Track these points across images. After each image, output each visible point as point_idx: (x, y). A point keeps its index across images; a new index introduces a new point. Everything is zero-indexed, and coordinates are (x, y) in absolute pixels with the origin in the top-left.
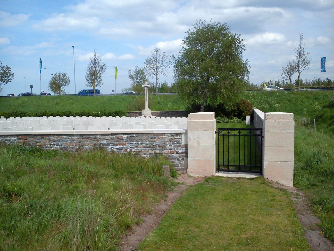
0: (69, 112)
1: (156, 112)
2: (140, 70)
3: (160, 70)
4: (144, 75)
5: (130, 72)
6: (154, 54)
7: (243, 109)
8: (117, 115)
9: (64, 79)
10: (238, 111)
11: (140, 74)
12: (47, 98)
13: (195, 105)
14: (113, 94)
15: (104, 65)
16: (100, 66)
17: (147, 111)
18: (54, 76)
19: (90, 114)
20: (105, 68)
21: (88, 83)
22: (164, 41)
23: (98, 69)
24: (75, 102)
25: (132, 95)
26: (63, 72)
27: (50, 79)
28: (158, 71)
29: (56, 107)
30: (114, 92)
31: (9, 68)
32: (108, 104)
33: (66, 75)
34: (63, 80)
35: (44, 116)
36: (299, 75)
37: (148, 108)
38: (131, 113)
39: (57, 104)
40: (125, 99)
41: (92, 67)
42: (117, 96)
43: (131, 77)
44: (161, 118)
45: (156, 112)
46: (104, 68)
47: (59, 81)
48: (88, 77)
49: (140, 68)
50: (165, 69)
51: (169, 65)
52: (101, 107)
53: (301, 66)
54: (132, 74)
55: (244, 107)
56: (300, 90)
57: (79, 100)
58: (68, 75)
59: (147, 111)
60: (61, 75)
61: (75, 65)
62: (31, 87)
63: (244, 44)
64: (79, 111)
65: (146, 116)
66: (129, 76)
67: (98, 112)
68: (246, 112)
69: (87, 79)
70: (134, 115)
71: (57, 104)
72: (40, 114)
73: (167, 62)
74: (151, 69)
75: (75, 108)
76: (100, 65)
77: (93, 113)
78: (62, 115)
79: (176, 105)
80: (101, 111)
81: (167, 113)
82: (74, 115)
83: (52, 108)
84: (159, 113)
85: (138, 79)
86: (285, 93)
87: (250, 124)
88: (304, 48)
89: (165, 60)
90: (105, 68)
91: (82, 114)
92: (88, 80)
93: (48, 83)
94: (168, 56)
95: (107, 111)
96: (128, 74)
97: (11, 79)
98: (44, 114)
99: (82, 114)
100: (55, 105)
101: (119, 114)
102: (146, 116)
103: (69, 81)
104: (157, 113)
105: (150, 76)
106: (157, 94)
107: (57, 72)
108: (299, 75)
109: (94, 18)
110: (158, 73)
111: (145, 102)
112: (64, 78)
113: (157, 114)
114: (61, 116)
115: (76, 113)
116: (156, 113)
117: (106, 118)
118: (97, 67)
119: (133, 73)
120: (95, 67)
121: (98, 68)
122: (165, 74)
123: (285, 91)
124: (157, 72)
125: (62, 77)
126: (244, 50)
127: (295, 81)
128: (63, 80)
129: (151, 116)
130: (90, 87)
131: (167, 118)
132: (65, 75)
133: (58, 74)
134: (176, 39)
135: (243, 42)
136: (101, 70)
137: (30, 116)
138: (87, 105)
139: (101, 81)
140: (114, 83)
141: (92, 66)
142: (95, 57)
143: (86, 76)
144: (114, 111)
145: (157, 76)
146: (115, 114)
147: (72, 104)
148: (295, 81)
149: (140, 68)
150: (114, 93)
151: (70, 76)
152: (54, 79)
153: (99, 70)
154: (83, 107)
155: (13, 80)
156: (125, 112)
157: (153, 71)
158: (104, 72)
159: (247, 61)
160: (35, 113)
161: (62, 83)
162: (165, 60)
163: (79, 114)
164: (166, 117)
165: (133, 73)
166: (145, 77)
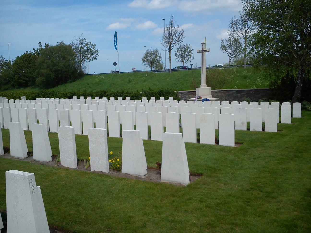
1: (223, 92)
13: (225, 70)
23: (174, 38)
31: (94, 46)
37: (206, 85)
38: (185, 93)
39: (130, 81)
42: (195, 70)
45: (222, 92)
58: (159, 51)
64: (156, 89)
70: (190, 95)
71: (130, 81)
81: (256, 92)
96: (221, 46)
97: (97, 57)
106: (245, 65)
107: (149, 49)
111: (201, 74)
116: (222, 93)
119: (226, 43)
132: (157, 51)
147: (145, 81)
155: (98, 57)
164: (240, 100)
165: (226, 43)
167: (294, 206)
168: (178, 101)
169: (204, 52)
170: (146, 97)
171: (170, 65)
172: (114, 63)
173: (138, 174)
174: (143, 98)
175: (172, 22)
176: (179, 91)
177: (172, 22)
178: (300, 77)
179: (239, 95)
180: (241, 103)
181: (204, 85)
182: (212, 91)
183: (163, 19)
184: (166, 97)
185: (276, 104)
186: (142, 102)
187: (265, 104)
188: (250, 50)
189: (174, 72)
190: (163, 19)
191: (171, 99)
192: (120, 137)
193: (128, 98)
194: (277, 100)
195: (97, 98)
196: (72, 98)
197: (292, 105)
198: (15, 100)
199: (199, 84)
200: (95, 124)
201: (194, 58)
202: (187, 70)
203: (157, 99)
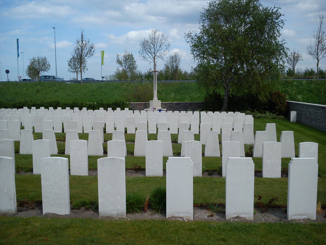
0: (56, 102)
1: (165, 104)
2: (129, 55)
3: (158, 54)
4: (134, 60)
5: (118, 57)
6: (152, 35)
7: (276, 101)
8: (118, 107)
9: (44, 64)
10: (269, 104)
11: (129, 59)
12: (26, 85)
14: (103, 81)
15: (92, 48)
16: (88, 49)
17: (156, 103)
18: (33, 61)
19: (83, 105)
20: (94, 51)
21: (70, 68)
22: (136, 30)
23: (85, 51)
24: (59, 89)
25: (125, 82)
26: (42, 55)
27: (27, 64)
28: (156, 55)
29: (36, 95)
30: (103, 78)
32: (98, 93)
33: (46, 59)
34: (43, 65)
35: (24, 107)
36: (318, 62)
38: (134, 105)
40: (117, 87)
41: (78, 49)
43: (119, 62)
44: (180, 112)
46: (92, 50)
47: (39, 66)
48: (70, 61)
49: (129, 53)
50: (164, 53)
51: (168, 48)
52: (90, 95)
53: (320, 53)
54: (120, 59)
55: (277, 99)
56: (318, 79)
57: (64, 87)
58: (48, 60)
59: (156, 103)
60: (41, 59)
61: (55, 48)
62: (7, 72)
63: (282, 20)
64: (112, 100)
65: (155, 109)
66: (117, 62)
67: (93, 102)
68: (280, 105)
69: (69, 65)
70: (138, 106)
71: (38, 91)
72: (19, 104)
73: (166, 45)
74: (148, 53)
75: (59, 96)
76: (88, 46)
77: (87, 104)
78: (47, 106)
79: (178, 95)
80: (97, 102)
81: (190, 104)
82: (63, 105)
83: (31, 96)
84: (168, 105)
85: (127, 64)
86: (303, 83)
87: (296, 121)
88: (324, 33)
89: (164, 43)
90: (94, 51)
91: (73, 104)
92: (71, 65)
93: (26, 68)
94: (167, 39)
95: (105, 102)
96: (116, 60)
98: (24, 105)
99: (73, 104)
100: (36, 93)
101: (121, 106)
102: (155, 109)
103: (50, 66)
104: (166, 104)
105: (146, 61)
108: (318, 62)
109: (66, 6)
110: (156, 57)
112: (43, 63)
113: (166, 105)
114: (47, 107)
115: (65, 103)
116: (165, 105)
117: (69, 110)
118: (84, 49)
119: (121, 58)
120: (82, 50)
121: (85, 50)
122: (163, 59)
123: (304, 81)
124: (155, 57)
125: (42, 61)
126: (282, 28)
127: (287, 70)
128: (43, 65)
129: (160, 108)
130: (73, 73)
131: (134, 111)
132: (45, 59)
133: (37, 59)
134: (148, 29)
135: (282, 18)
136: (89, 53)
137: (6, 108)
138: (73, 93)
139: (86, 67)
140: (101, 68)
141: (79, 48)
142: (82, 38)
143: (69, 61)
144: (114, 102)
145: (154, 61)
146: (116, 105)
147: (56, 91)
148: (287, 70)
149: (129, 53)
150: (104, 79)
151: (51, 61)
152: (33, 63)
153: (86, 53)
154: (69, 95)
156: (127, 103)
157: (150, 54)
158: (93, 55)
159: (284, 42)
160: (13, 103)
161: (41, 68)
162: (164, 43)
163: (70, 106)
164: (186, 110)
165: (121, 58)
166: (135, 63)
167: (79, 226)
168: (12, 109)
169: (156, 72)
170: (103, 108)
171: (81, 77)
172: (9, 73)
173: (252, 144)
174: (100, 108)
175: (82, 36)
176: (130, 103)
177: (82, 36)
178: (226, 94)
179: (178, 107)
180: (214, 112)
181: (156, 98)
182: (161, 103)
183: (54, 28)
184: (122, 108)
185: (197, 113)
186: (48, 110)
187: (190, 113)
188: (120, 60)
189: (86, 84)
190: (54, 28)
191: (127, 109)
192: (156, 133)
193: (84, 109)
194: (197, 110)
195: (109, 109)
196: (124, 109)
197: (200, 113)
198: (134, 111)
199: (152, 98)
200: (92, 128)
201: (88, 70)
202: (98, 82)
203: (114, 109)
